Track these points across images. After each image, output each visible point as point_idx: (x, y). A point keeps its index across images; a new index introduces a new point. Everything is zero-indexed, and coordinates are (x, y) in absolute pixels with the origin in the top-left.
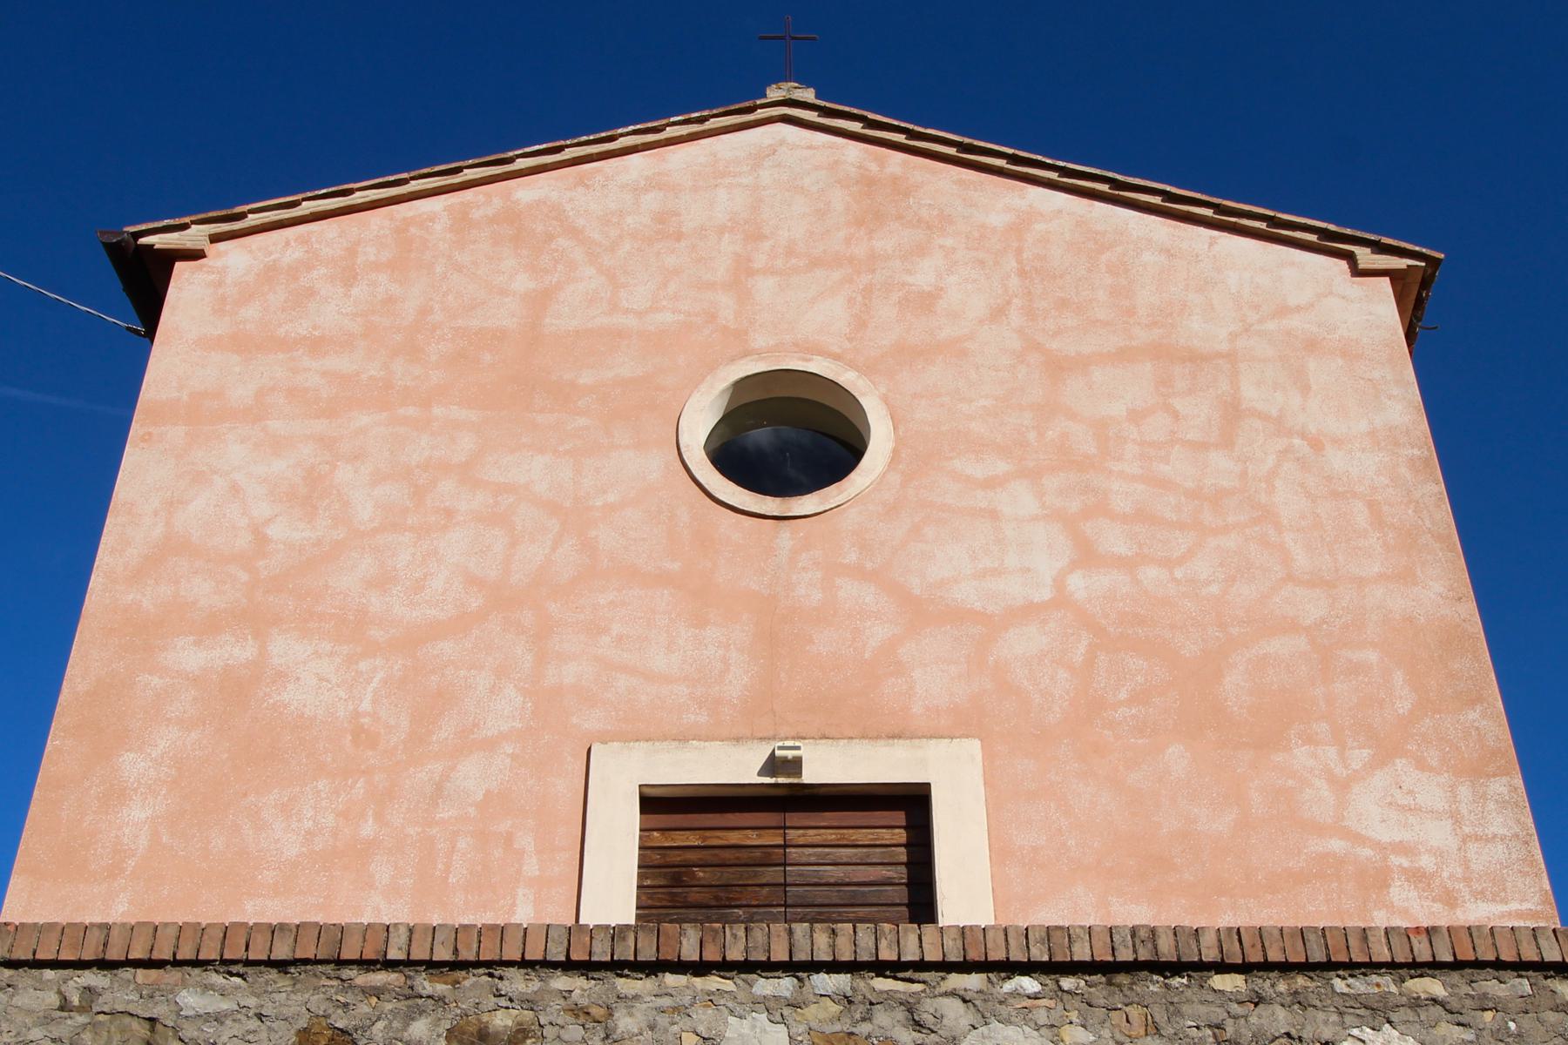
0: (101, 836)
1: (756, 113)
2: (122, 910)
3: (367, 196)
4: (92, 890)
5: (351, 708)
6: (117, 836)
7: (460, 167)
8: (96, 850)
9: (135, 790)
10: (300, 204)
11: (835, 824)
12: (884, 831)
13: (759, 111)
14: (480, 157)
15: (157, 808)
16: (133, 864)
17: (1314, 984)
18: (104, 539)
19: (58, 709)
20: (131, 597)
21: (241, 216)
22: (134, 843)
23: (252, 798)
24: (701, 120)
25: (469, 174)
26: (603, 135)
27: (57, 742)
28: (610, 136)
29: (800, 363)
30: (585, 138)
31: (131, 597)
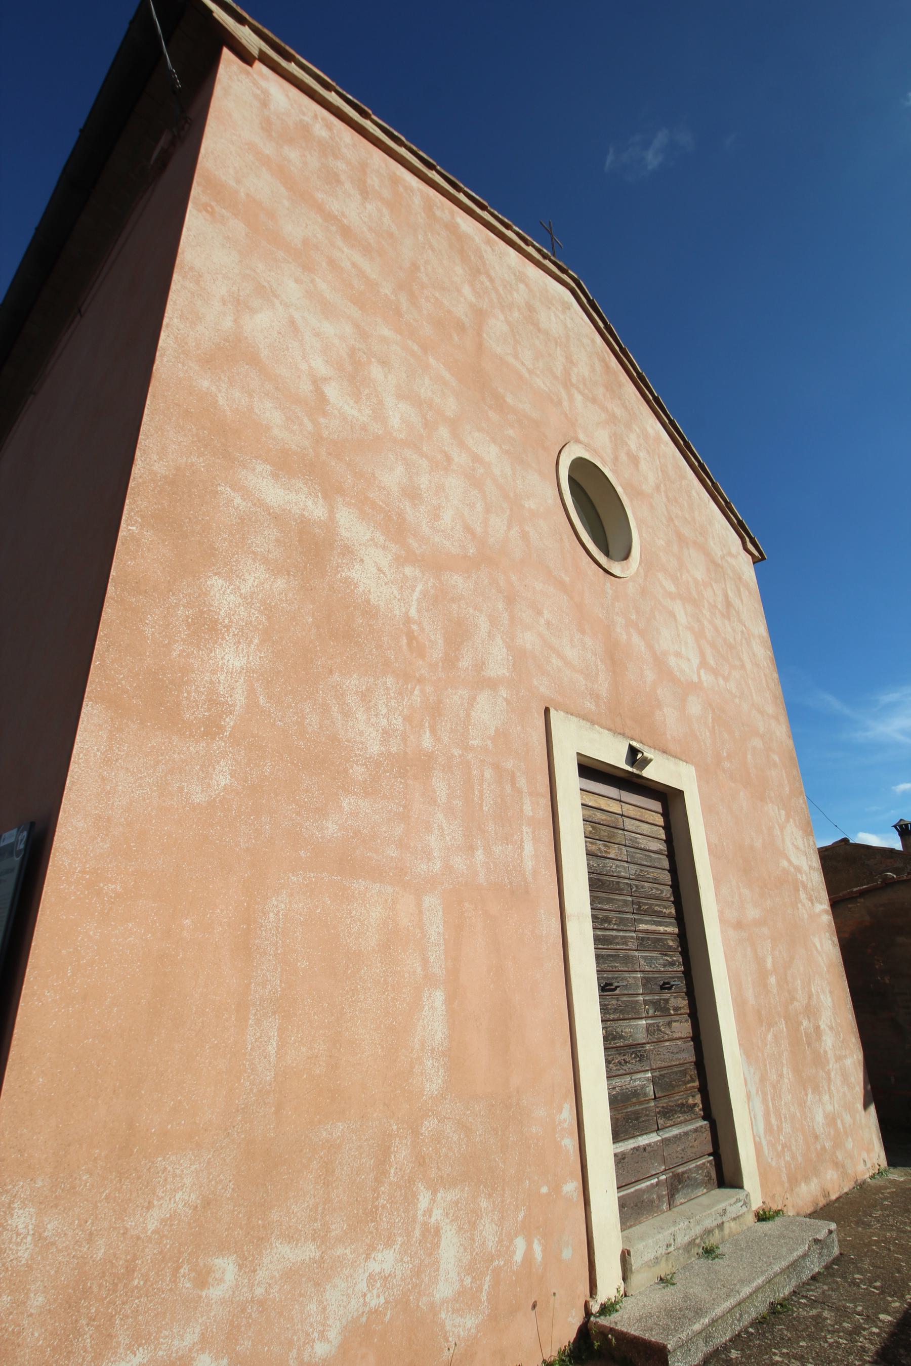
0: (194, 675)
1: (431, 171)
2: (223, 784)
3: (375, 131)
4: (188, 748)
5: (404, 609)
6: (211, 682)
7: (245, 19)
8: (189, 693)
9: (228, 627)
10: (330, 91)
11: (639, 804)
12: (654, 814)
13: (486, 212)
14: (445, 169)
15: (251, 659)
16: (232, 724)
17: (276, 1232)
18: (172, 296)
19: (132, 484)
20: (206, 384)
21: (289, 58)
22: (231, 696)
23: (336, 677)
24: (545, 257)
25: (333, 97)
26: (506, 220)
27: (134, 528)
28: (508, 224)
29: (602, 465)
30: (496, 213)
31: (206, 384)
